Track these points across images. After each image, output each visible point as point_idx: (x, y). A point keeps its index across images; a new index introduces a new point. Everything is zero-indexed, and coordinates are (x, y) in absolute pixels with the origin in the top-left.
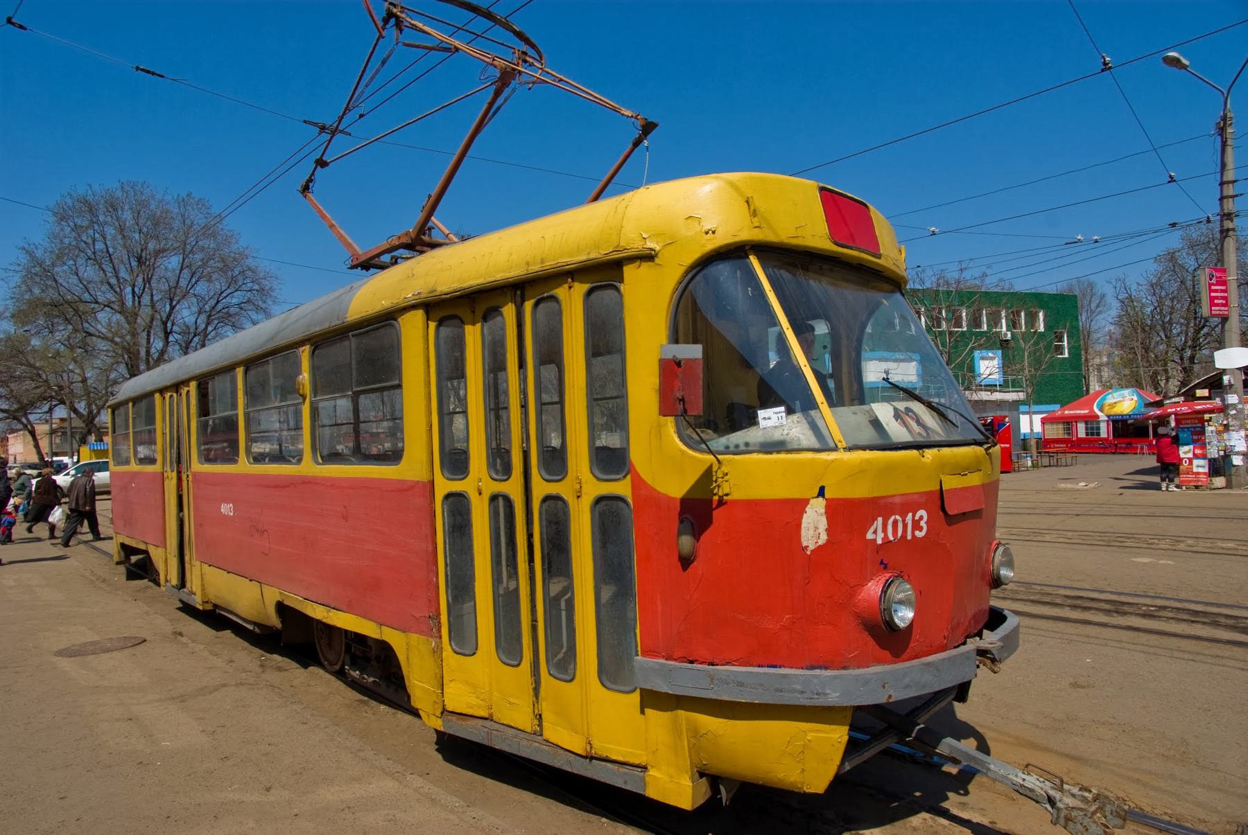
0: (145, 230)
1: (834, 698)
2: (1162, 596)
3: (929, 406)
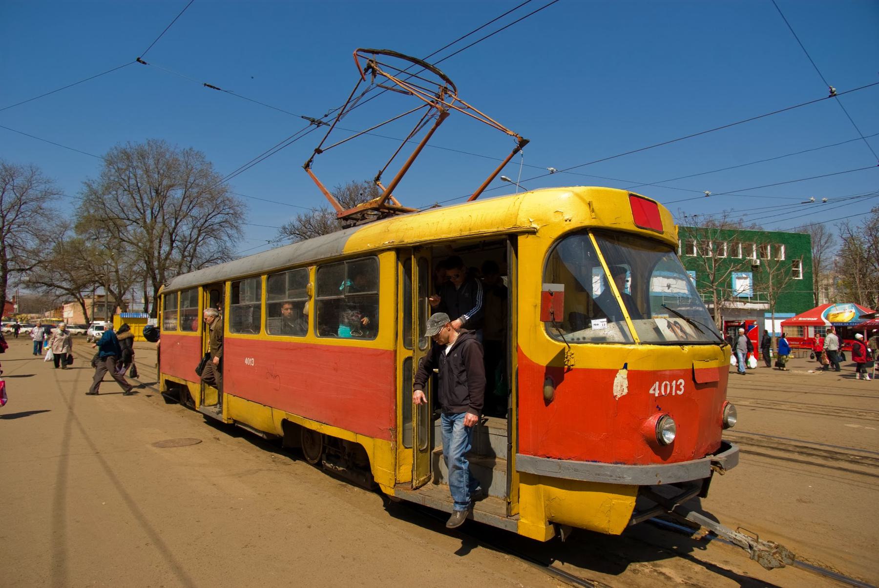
0: (162, 172)
1: (628, 480)
2: (865, 450)
3: (688, 321)
